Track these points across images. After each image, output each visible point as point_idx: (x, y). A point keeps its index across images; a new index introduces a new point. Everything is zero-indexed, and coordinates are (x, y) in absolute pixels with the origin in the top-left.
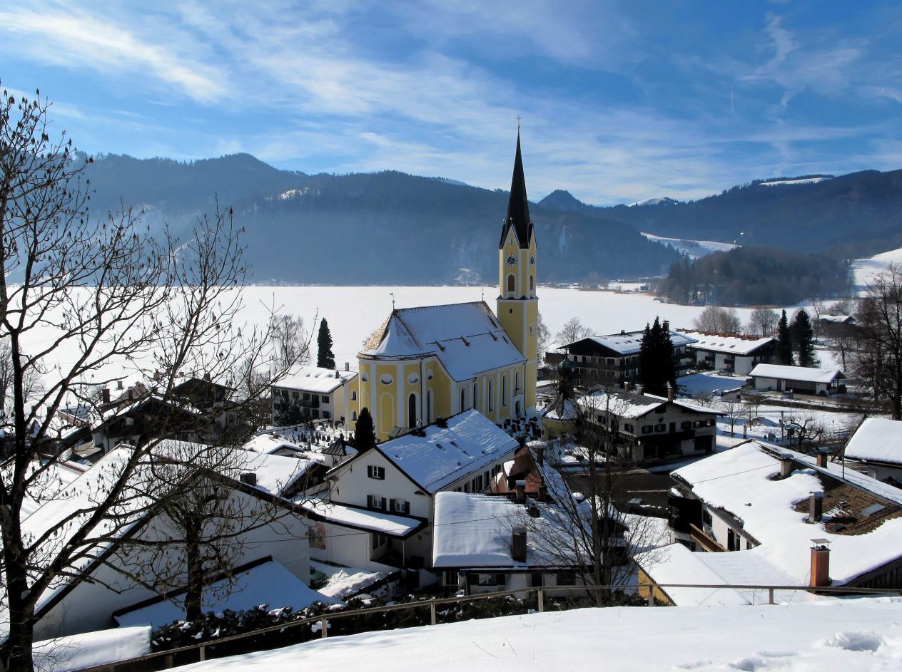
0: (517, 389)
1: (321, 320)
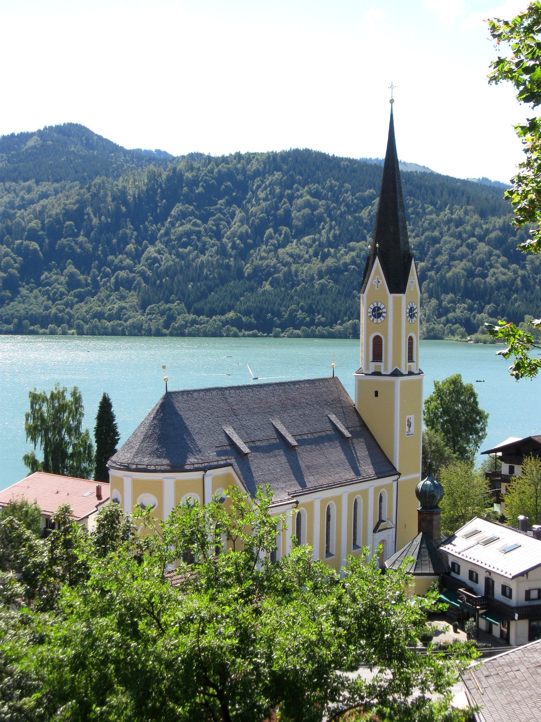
0: (381, 521)
1: (100, 399)
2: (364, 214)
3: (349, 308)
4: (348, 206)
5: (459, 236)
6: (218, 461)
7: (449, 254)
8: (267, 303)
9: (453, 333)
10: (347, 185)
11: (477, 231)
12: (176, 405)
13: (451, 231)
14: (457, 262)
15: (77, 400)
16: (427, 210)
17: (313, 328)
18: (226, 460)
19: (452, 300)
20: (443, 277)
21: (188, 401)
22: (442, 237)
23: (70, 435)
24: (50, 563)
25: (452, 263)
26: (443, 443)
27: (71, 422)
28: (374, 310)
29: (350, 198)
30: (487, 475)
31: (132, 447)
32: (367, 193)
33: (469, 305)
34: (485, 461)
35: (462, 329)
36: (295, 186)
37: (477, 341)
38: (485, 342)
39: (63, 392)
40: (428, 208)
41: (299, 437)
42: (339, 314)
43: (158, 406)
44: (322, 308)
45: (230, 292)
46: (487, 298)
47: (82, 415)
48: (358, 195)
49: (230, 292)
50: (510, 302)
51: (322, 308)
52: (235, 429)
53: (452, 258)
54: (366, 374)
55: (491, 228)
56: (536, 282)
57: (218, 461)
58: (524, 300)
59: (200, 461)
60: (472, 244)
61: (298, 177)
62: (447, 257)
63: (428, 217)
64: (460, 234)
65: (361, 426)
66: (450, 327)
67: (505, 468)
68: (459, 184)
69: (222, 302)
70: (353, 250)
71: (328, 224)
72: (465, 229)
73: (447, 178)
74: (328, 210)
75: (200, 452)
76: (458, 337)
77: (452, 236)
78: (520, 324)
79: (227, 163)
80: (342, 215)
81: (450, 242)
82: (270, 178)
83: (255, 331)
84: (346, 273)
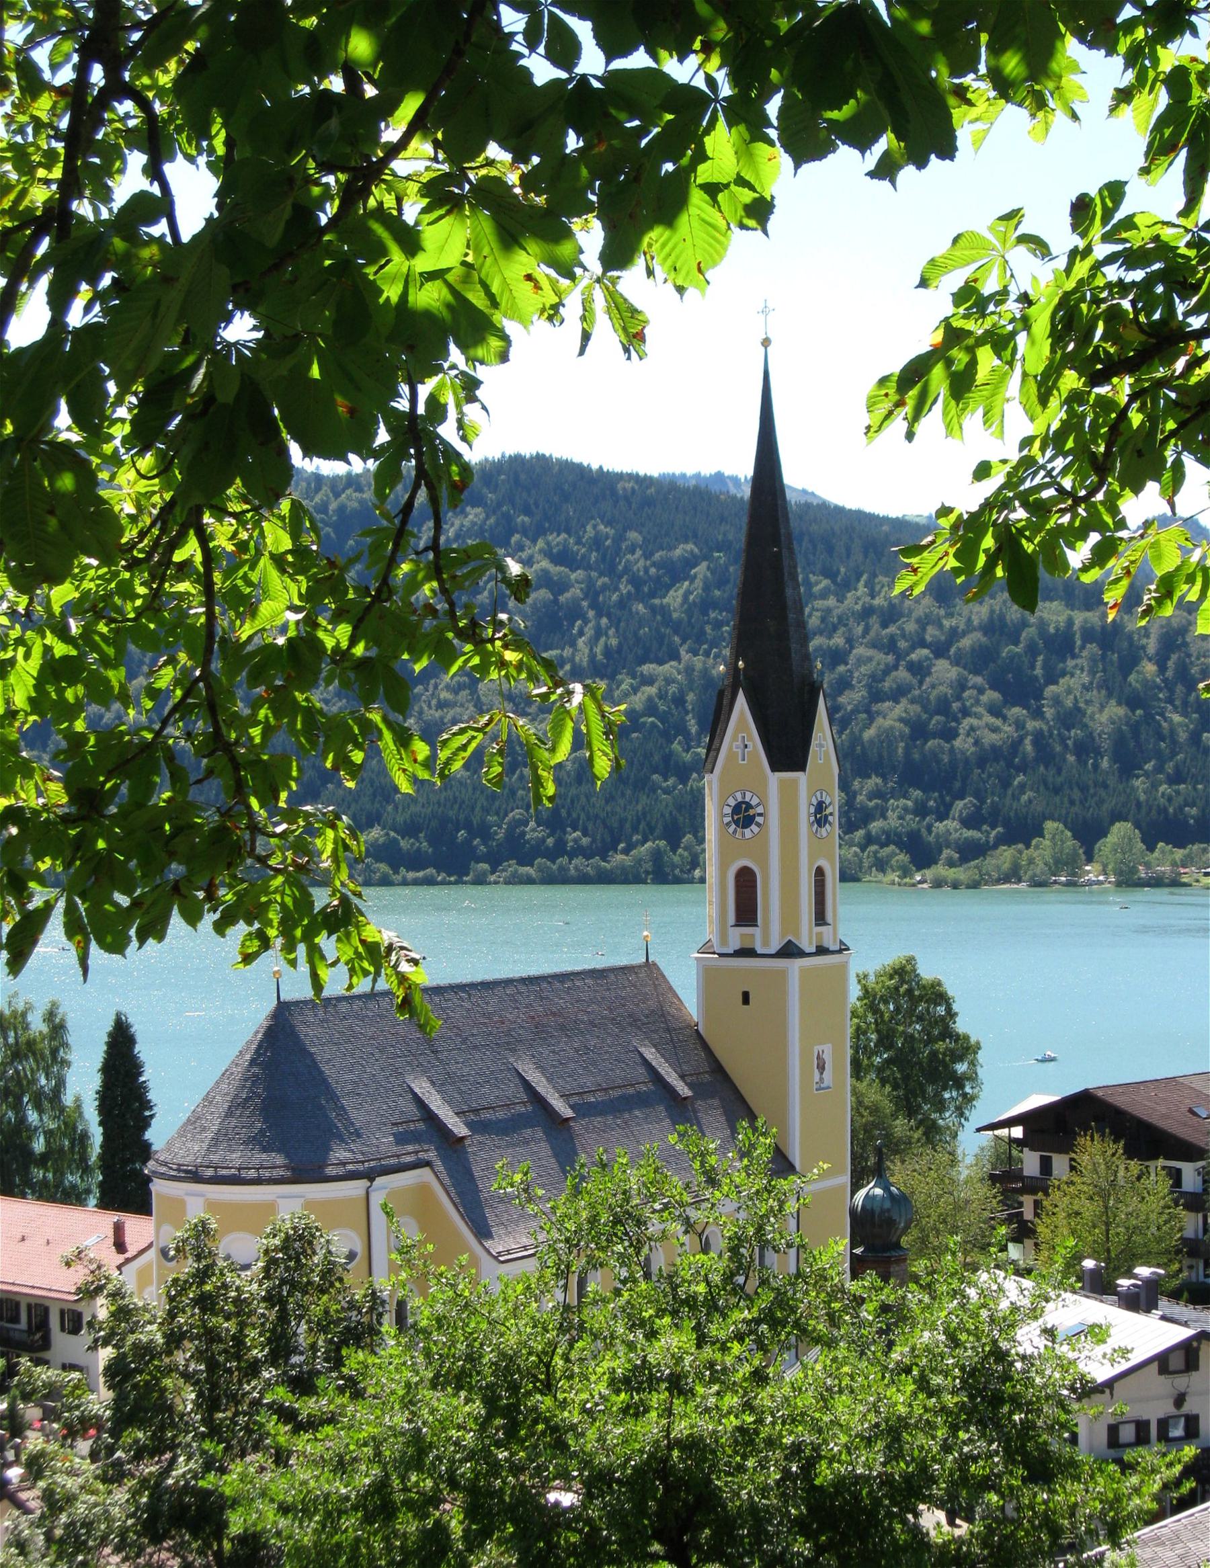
1: (109, 1025)
2: (674, 598)
3: (644, 814)
4: (636, 581)
5: (890, 646)
6: (398, 1156)
7: (869, 687)
8: (456, 807)
9: (881, 865)
10: (633, 536)
11: (931, 633)
12: (302, 1030)
13: (872, 634)
14: (887, 704)
15: (57, 1029)
16: (816, 589)
17: (562, 861)
18: (417, 1152)
19: (879, 791)
20: (856, 740)
21: (327, 1021)
22: (852, 648)
23: (39, 1109)
24: (167, 1343)
25: (874, 708)
26: (888, 1106)
27: (43, 1081)
28: (737, 809)
29: (641, 563)
30: (993, 1178)
31: (204, 1129)
32: (678, 552)
33: (916, 802)
34: (982, 1149)
35: (903, 858)
36: (516, 538)
37: (938, 884)
38: (955, 886)
39: (24, 1015)
40: (817, 583)
41: (575, 1099)
42: (621, 826)
43: (260, 1036)
44: (583, 816)
45: (372, 782)
46: (957, 785)
47: (65, 1063)
48: (657, 556)
49: (372, 782)
50: (1010, 792)
51: (583, 816)
52: (433, 1083)
53: (876, 696)
54: (721, 955)
55: (962, 626)
56: (1066, 746)
57: (398, 1156)
58: (1042, 788)
59: (361, 1158)
60: (920, 662)
61: (523, 519)
62: (864, 693)
63: (819, 604)
64: (892, 640)
65: (712, 1072)
66: (876, 853)
67: (1030, 1163)
68: (885, 528)
69: (353, 806)
70: (649, 681)
71: (590, 625)
72: (902, 630)
73: (860, 516)
74: (592, 593)
75: (359, 1136)
76: (894, 876)
77: (874, 645)
78: (1034, 842)
79: (359, 489)
80: (623, 604)
81: (870, 659)
82: (457, 522)
83: (430, 871)
84: (635, 735)
